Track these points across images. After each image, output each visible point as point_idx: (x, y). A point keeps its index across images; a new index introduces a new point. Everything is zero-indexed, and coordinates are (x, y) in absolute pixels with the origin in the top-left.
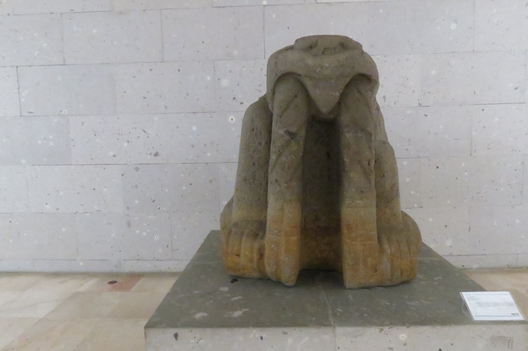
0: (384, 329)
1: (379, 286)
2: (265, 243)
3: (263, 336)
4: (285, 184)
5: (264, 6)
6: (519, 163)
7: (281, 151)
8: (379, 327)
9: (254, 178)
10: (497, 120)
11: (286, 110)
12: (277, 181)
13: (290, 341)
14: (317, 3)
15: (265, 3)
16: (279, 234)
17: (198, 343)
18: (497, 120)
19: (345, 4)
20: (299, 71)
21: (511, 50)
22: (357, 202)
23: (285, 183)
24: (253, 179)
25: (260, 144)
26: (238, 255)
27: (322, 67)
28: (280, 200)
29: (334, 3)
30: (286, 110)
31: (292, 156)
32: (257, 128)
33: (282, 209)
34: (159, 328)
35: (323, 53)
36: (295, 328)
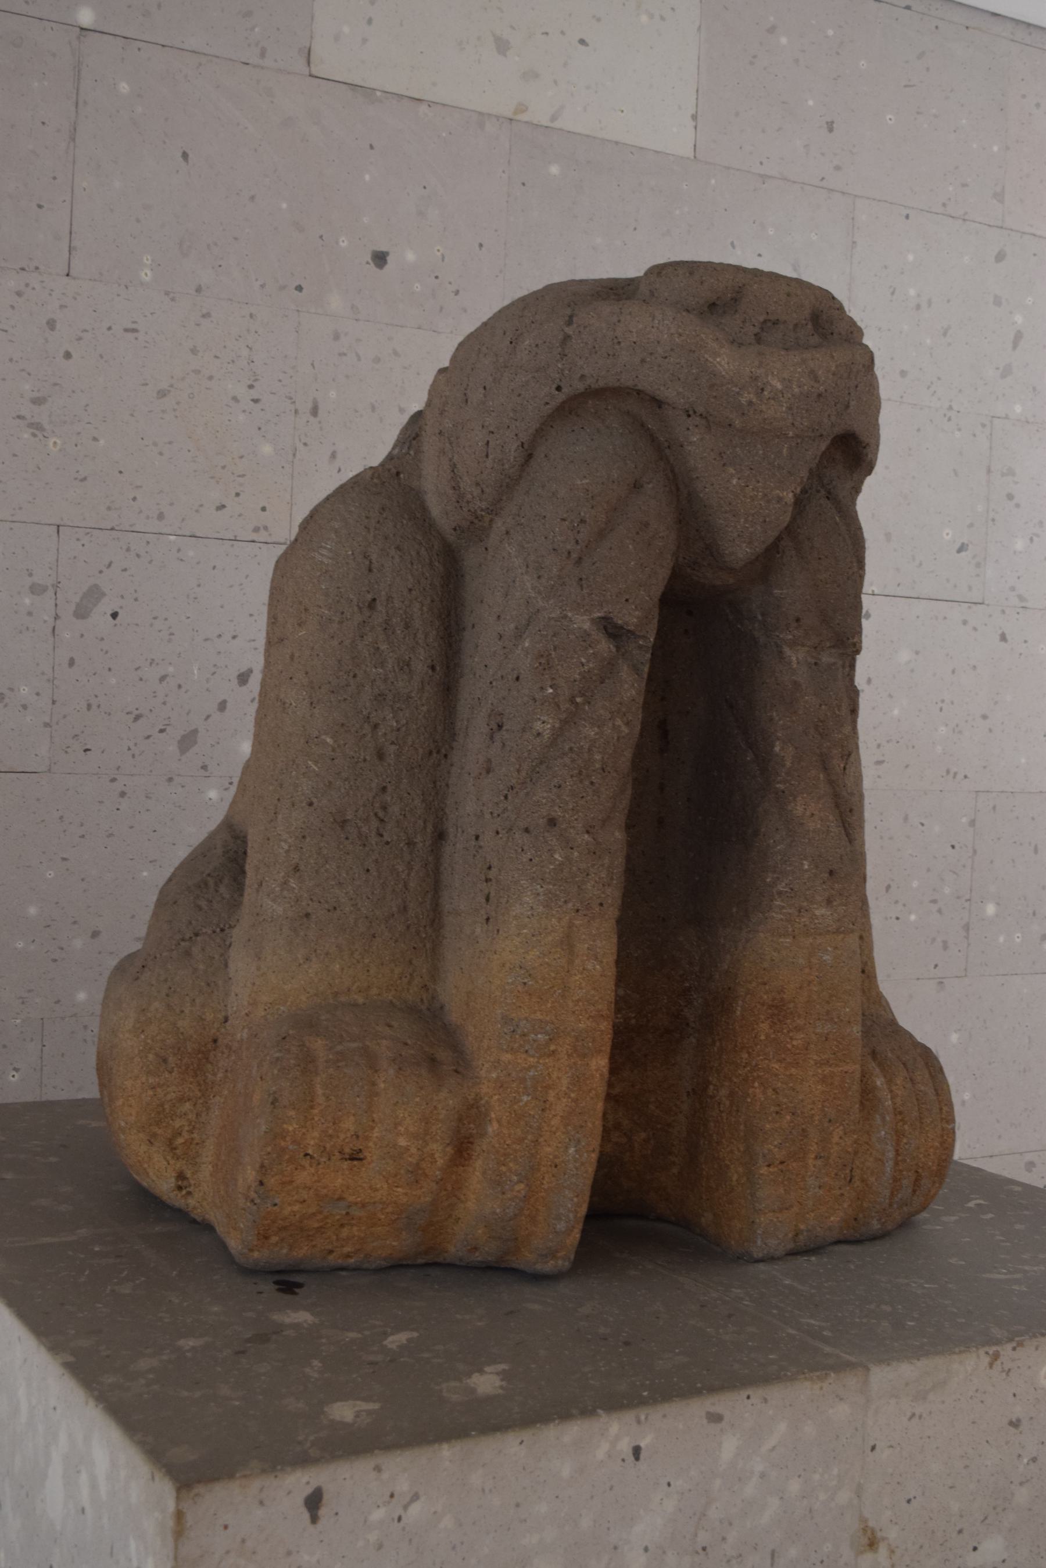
0: (1002, 1353)
1: (838, 1242)
2: (485, 1089)
3: (642, 1445)
4: (586, 836)
5: (82, 29)
6: (964, 820)
7: (579, 700)
8: (987, 1349)
9: (381, 814)
10: (904, 656)
11: (601, 535)
12: (552, 822)
13: (729, 1446)
14: (311, 75)
15: (86, 17)
16: (552, 1047)
17: (400, 1519)
18: (904, 656)
19: (423, 108)
20: (669, 393)
21: (950, 408)
22: (817, 912)
23: (588, 832)
24: (375, 823)
25: (405, 666)
26: (355, 1157)
27: (763, 390)
28: (566, 902)
29: (378, 94)
30: (601, 535)
31: (619, 722)
32: (389, 599)
33: (567, 943)
34: (245, 1476)
35: (758, 339)
36: (749, 1392)
